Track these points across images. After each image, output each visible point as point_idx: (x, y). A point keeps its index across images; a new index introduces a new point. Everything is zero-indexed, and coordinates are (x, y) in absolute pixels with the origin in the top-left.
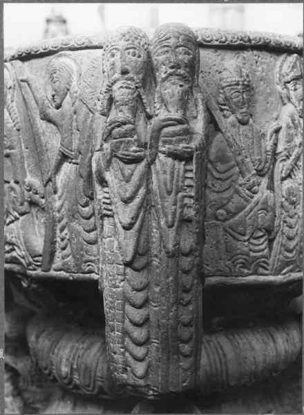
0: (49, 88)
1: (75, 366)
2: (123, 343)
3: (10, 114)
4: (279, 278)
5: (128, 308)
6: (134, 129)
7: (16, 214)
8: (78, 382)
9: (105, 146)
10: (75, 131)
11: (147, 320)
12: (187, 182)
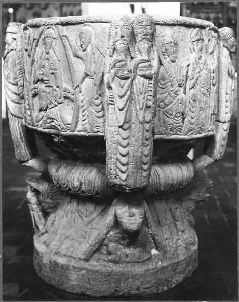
0: (78, 41)
1: (83, 182)
2: (116, 164)
3: (55, 53)
4: (187, 137)
5: (120, 148)
6: (126, 63)
7: (56, 103)
8: (84, 190)
9: (112, 71)
10: (93, 63)
11: (128, 153)
12: (150, 89)
